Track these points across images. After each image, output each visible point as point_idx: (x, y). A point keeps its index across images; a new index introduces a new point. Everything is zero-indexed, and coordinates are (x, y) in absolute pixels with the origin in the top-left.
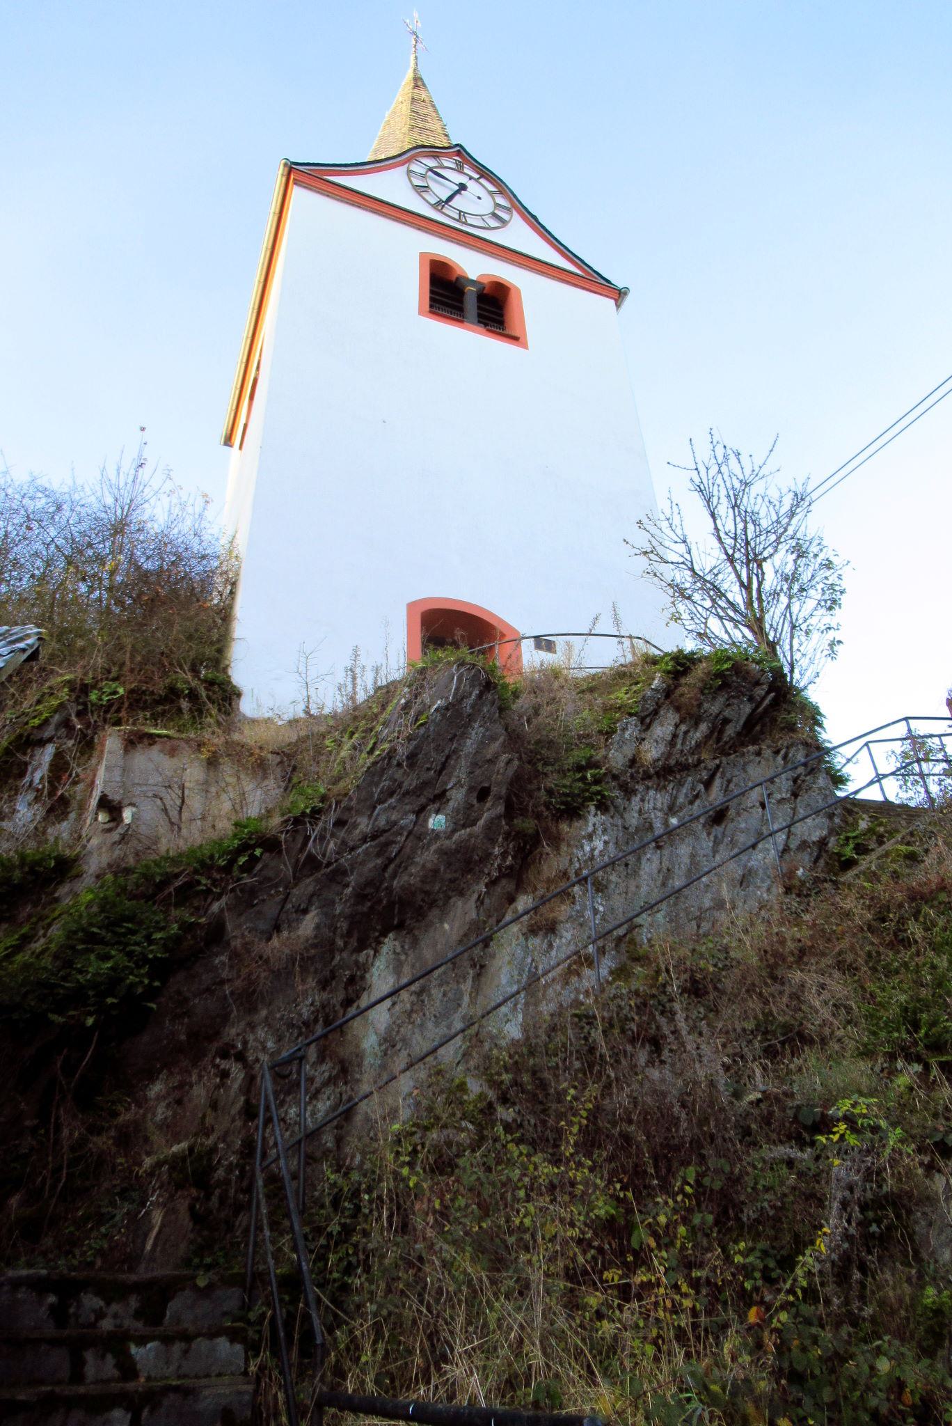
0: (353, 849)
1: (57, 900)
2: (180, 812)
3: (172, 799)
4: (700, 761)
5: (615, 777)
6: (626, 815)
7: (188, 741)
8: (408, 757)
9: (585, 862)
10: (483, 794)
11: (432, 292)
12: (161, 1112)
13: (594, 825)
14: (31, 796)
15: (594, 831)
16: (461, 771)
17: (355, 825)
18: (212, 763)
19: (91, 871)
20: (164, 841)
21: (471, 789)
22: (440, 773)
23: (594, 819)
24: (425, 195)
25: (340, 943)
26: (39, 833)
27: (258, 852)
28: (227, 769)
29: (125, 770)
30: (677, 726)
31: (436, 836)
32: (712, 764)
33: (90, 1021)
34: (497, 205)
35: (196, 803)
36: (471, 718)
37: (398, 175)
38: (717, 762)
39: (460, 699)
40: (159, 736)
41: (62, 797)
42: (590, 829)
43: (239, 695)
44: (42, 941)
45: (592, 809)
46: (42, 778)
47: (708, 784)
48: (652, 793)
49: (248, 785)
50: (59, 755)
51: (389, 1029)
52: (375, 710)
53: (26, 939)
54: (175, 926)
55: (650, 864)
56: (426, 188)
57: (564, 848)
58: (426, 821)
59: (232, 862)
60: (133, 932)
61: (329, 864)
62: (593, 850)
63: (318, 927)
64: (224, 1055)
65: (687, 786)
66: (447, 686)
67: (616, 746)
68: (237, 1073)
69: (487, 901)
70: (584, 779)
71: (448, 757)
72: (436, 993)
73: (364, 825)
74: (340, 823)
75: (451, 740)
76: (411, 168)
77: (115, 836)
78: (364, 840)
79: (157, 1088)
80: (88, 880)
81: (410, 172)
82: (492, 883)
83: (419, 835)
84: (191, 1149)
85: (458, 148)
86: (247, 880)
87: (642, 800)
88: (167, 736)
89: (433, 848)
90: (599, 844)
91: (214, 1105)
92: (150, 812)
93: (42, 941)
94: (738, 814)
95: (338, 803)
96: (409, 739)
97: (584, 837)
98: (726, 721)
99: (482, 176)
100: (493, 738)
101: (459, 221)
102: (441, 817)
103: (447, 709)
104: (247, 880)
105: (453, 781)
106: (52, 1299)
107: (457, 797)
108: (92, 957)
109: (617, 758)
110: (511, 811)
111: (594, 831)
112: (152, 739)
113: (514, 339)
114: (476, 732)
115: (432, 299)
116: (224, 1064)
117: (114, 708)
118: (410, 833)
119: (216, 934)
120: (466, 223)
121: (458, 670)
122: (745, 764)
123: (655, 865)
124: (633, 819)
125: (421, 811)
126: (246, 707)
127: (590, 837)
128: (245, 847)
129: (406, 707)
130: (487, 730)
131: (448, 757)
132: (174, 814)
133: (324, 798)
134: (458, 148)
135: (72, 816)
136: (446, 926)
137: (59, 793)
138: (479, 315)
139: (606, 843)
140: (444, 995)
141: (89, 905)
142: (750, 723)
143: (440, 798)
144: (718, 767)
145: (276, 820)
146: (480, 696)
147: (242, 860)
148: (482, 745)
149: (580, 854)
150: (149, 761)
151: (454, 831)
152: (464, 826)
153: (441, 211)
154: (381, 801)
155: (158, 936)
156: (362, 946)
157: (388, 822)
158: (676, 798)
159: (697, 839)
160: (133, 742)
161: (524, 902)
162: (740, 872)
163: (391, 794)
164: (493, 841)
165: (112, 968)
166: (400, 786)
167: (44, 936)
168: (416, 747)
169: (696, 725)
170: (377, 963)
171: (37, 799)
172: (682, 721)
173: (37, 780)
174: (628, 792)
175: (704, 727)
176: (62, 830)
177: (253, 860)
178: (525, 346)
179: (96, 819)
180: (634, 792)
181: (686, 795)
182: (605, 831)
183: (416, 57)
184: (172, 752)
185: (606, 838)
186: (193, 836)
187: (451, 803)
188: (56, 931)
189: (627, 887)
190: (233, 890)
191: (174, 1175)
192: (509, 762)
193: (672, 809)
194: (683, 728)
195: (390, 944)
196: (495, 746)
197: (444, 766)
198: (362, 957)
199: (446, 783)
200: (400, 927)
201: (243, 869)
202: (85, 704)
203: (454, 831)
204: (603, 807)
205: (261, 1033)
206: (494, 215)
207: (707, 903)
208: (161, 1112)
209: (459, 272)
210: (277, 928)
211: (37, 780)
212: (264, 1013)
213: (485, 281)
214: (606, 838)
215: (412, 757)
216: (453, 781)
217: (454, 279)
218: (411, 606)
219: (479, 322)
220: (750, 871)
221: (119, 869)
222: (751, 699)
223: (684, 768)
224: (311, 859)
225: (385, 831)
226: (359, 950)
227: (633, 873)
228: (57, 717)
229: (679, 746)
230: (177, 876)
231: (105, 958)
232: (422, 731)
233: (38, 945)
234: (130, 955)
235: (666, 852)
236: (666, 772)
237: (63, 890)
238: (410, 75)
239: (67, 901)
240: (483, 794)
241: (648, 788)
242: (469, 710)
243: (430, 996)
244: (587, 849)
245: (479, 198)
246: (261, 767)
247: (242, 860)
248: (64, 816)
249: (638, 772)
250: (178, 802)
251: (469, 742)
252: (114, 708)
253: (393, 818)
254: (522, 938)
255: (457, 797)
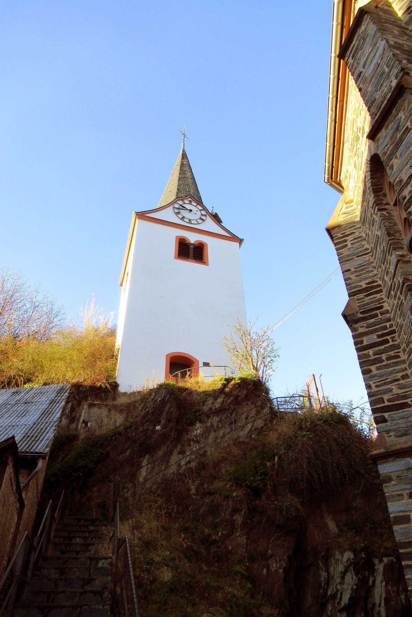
0: (138, 435)
1: (73, 446)
2: (101, 424)
3: (99, 421)
4: (230, 408)
5: (205, 414)
6: (207, 424)
7: (104, 405)
8: (152, 413)
9: (195, 436)
10: (169, 421)
11: (179, 247)
12: (96, 494)
13: (198, 426)
14: (66, 416)
15: (198, 428)
16: (164, 415)
17: (139, 429)
18: (110, 410)
19: (81, 438)
20: (97, 432)
21: (166, 420)
22: (159, 416)
23: (198, 425)
24: (179, 215)
25: (135, 456)
26: (68, 427)
27: (117, 436)
28: (113, 412)
29: (89, 413)
30: (224, 398)
31: (158, 431)
32: (232, 408)
33: (81, 474)
34: (202, 215)
35: (105, 420)
36: (167, 402)
37: (170, 209)
38: (234, 407)
39: (164, 397)
40: (97, 404)
41: (73, 417)
42: (197, 427)
43: (119, 386)
44: (70, 455)
45: (198, 422)
46: (68, 412)
47: (231, 414)
48: (215, 417)
49: (118, 415)
50: (72, 406)
51: (145, 476)
52: (148, 397)
53: (66, 455)
54: (99, 453)
55: (212, 436)
56: (179, 213)
57: (189, 433)
58: (156, 428)
59: (112, 438)
60: (90, 455)
61: (133, 439)
62: (197, 433)
63: (130, 453)
64: (109, 482)
65: (226, 414)
66: (162, 394)
67: (206, 405)
68: (112, 485)
69: (170, 446)
70: (196, 415)
71: (161, 412)
72: (157, 468)
73: (141, 429)
74: (136, 429)
75: (162, 408)
76: (174, 206)
77: (86, 429)
78: (141, 432)
79: (95, 489)
80: (80, 441)
81: (174, 208)
82: (172, 441)
83: (154, 430)
84: (101, 501)
85: (190, 196)
86: (115, 443)
87: (212, 419)
88: (98, 404)
89: (157, 434)
90: (199, 431)
91: (107, 492)
92: (94, 424)
93: (70, 455)
94: (239, 421)
95: (136, 424)
96: (152, 408)
97: (195, 430)
98: (239, 396)
99: (198, 204)
100: (172, 407)
101: (189, 223)
102: (159, 427)
103: (161, 400)
104: (115, 443)
105: (162, 418)
106: (76, 521)
107: (163, 422)
108: (82, 460)
109: (206, 408)
110: (177, 423)
111: (198, 428)
112: (95, 405)
113: (205, 263)
114: (168, 405)
115: (179, 253)
116: (109, 484)
117: (86, 392)
118: (152, 430)
119: (108, 455)
120: (191, 223)
121: (165, 390)
122: (243, 407)
123: (213, 437)
124: (209, 424)
125: (155, 426)
126: (122, 389)
127: (196, 430)
128: (115, 435)
129: (153, 399)
130: (171, 405)
131: (161, 412)
132: (100, 425)
133: (132, 423)
134: (190, 196)
135: (76, 421)
136: (160, 452)
137: (73, 416)
138: (194, 256)
139: (201, 431)
140: (158, 468)
141: (81, 447)
142: (246, 395)
143: (159, 423)
144: (235, 409)
145: (122, 428)
146: (169, 397)
147: (114, 438)
148: (169, 409)
149: (193, 434)
150: (95, 410)
151: (162, 430)
152: (165, 429)
153: (183, 220)
154: (145, 423)
155: (95, 455)
156: (141, 457)
157: (146, 428)
158: (222, 418)
159: (226, 428)
160: (91, 406)
161: (179, 447)
162: (236, 437)
163: (148, 422)
164: (172, 432)
165: (86, 463)
166: (150, 419)
167: (71, 454)
168: (154, 410)
169: (229, 398)
170: (144, 461)
171: (67, 417)
172: (226, 397)
173: (67, 412)
174: (208, 417)
175: (231, 398)
176: (74, 426)
177: (116, 438)
178: (208, 265)
179: (82, 425)
180: (210, 417)
181: (225, 417)
182: (201, 428)
183: (184, 144)
184: (100, 408)
185: (201, 430)
186: (104, 430)
187: (162, 423)
188: (73, 453)
189: (205, 442)
190: (112, 445)
191: (61, 364)
192: (176, 413)
193: (220, 421)
194: (226, 399)
195: (147, 457)
196: (172, 409)
197: (160, 414)
198: (140, 460)
199: (161, 419)
200: (150, 452)
201: (115, 440)
202: (79, 391)
203: (162, 430)
204: (200, 422)
205: (117, 477)
206: (201, 219)
207: (226, 445)
208: (96, 494)
209: (188, 242)
210: (121, 453)
211: (67, 412)
212: (118, 472)
213: (196, 243)
214: (201, 430)
215: (153, 413)
216: (162, 418)
217: (187, 243)
218: (167, 356)
219: (193, 258)
220: (239, 437)
221: (87, 438)
222: (247, 389)
223: (225, 410)
224: (129, 437)
225: (145, 431)
226: (140, 458)
227: (207, 438)
228: (72, 395)
229: (224, 404)
230: (100, 441)
231: (84, 460)
232: (155, 406)
233: (69, 456)
234: (90, 460)
235: (216, 433)
236: (218, 412)
237: (75, 443)
238: (181, 152)
239: (76, 446)
240: (169, 421)
241: (214, 416)
242: (167, 400)
243: (155, 468)
244: (195, 433)
245: (197, 211)
246: (121, 411)
247: (114, 438)
248: (74, 422)
249: (211, 412)
250: (101, 422)
251: (166, 408)
252: (86, 392)
253: (148, 427)
254: (177, 455)
255: (163, 422)
